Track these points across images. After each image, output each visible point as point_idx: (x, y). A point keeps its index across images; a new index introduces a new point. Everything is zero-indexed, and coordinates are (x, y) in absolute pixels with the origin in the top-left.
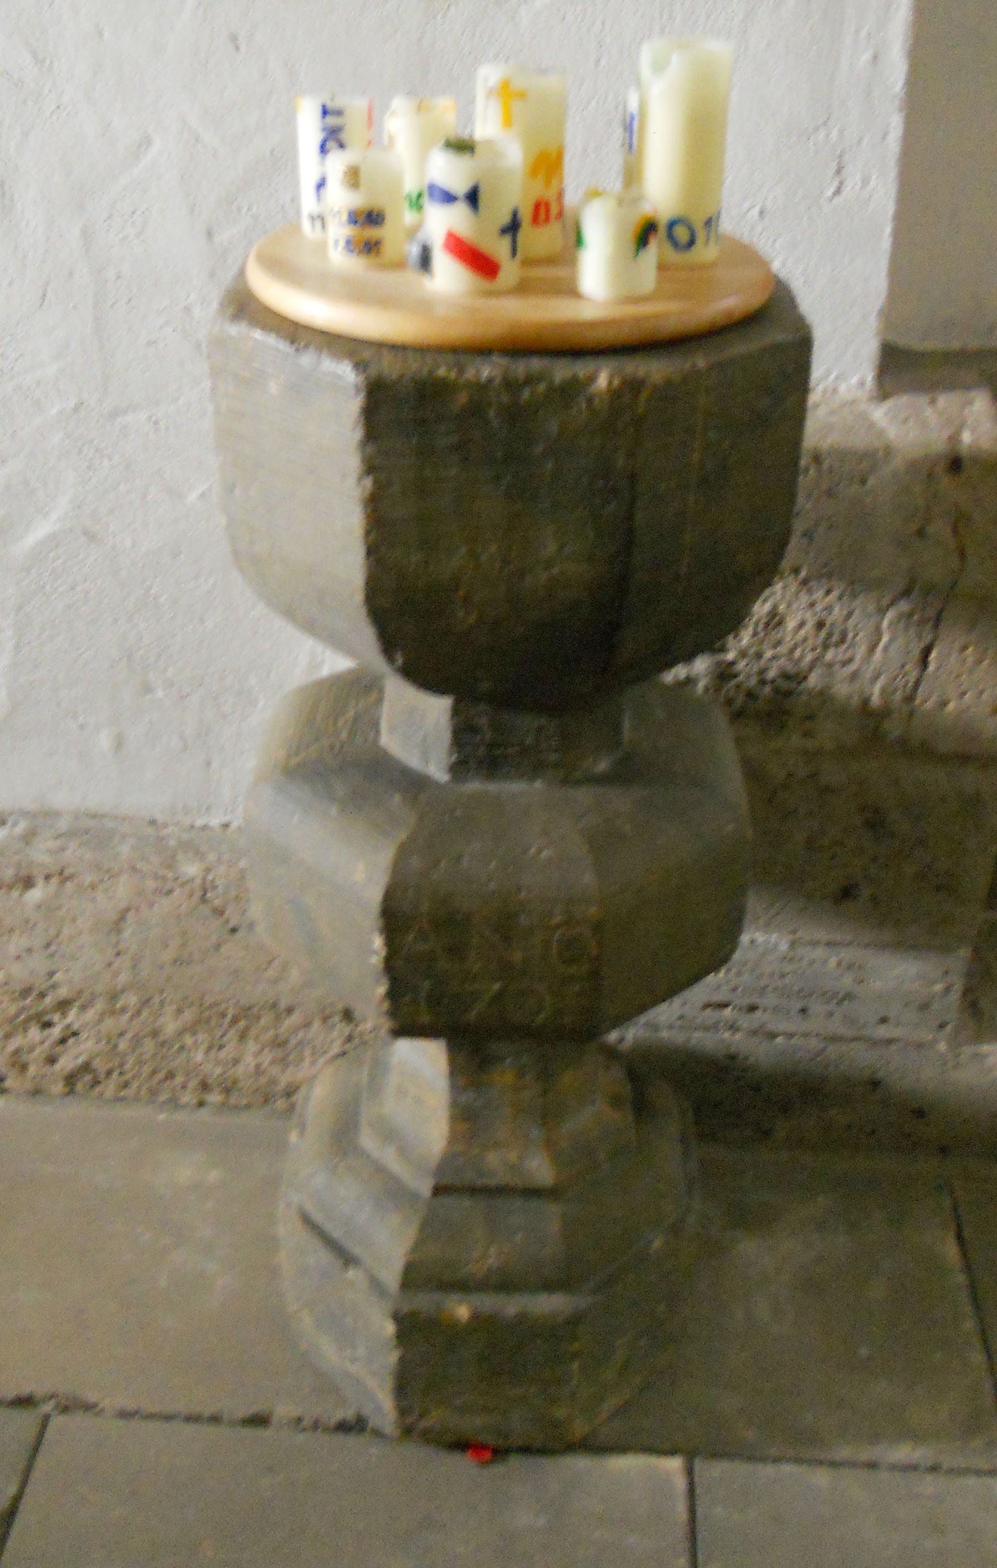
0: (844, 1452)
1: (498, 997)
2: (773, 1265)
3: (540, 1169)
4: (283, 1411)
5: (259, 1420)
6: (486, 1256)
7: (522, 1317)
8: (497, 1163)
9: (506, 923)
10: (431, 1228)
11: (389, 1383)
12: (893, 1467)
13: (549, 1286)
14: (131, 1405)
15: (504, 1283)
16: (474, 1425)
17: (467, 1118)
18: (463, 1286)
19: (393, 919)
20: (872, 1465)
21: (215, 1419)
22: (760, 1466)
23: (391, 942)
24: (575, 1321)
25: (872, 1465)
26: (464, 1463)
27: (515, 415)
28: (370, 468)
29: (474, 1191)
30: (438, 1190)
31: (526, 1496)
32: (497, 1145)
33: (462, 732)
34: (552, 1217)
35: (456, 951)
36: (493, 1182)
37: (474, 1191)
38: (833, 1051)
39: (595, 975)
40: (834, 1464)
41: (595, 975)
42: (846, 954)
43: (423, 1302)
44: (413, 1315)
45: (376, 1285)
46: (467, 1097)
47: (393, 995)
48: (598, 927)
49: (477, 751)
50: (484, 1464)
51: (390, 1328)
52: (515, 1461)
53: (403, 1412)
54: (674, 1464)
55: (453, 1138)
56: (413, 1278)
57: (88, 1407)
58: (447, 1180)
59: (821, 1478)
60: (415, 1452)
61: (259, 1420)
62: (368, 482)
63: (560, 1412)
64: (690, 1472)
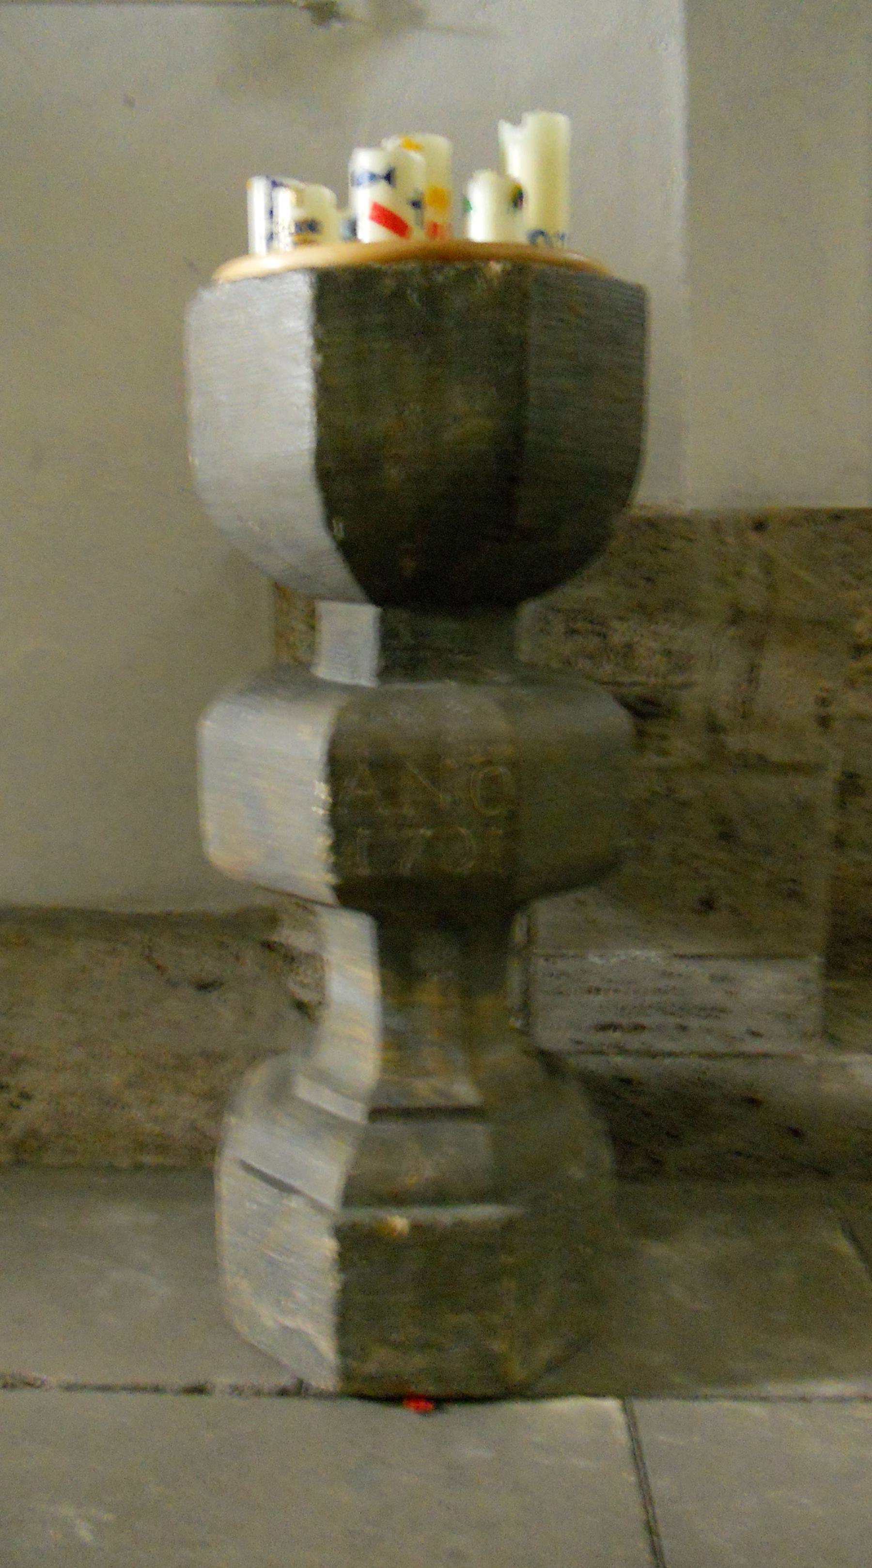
0: (774, 1388)
1: (430, 844)
2: (683, 1262)
3: (465, 1092)
4: (222, 1380)
5: (198, 1390)
6: (419, 1168)
7: (459, 1224)
8: (424, 1090)
9: (433, 764)
10: (366, 1145)
11: (328, 1318)
12: (826, 1399)
13: (480, 1197)
14: (72, 1379)
15: (439, 1196)
16: (413, 1365)
17: (397, 1043)
18: (399, 1199)
19: (337, 768)
20: (803, 1399)
21: (157, 1389)
22: (696, 1404)
23: (336, 791)
24: (509, 1226)
25: (803, 1399)
26: (403, 1419)
27: (432, 297)
28: (320, 346)
29: (407, 1114)
30: (376, 1114)
31: (471, 1436)
32: (428, 1074)
33: (388, 637)
34: (478, 1134)
35: (391, 795)
36: (423, 1104)
37: (407, 1114)
38: (716, 1067)
39: (512, 817)
40: (764, 1399)
41: (512, 817)
42: (716, 967)
43: (363, 1215)
44: (353, 1227)
45: (318, 1208)
46: (396, 1022)
47: (336, 848)
48: (513, 765)
49: (401, 658)
50: (424, 1413)
51: (329, 1246)
52: (457, 1414)
53: (344, 1352)
54: (610, 1405)
55: (385, 1069)
56: (354, 1193)
57: (29, 1384)
58: (384, 1103)
59: (757, 1410)
60: (356, 1407)
61: (198, 1390)
62: (319, 359)
63: (498, 1346)
64: (627, 1411)
